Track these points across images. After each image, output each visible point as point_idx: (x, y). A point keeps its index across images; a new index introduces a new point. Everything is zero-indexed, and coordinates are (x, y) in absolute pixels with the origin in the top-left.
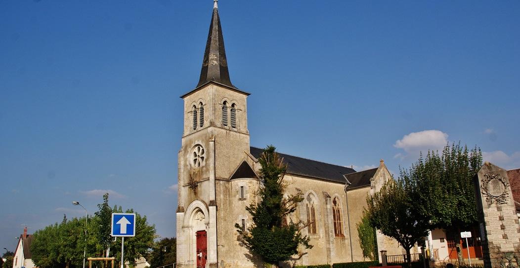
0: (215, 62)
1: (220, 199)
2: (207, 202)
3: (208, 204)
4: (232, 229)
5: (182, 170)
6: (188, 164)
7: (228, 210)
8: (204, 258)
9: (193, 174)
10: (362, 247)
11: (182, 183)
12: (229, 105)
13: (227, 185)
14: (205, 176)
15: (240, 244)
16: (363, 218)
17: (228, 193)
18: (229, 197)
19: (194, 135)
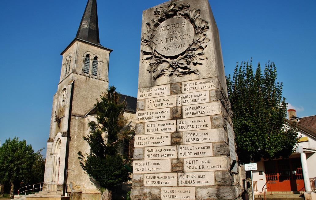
0: (86, 26)
12: (92, 57)
13: (82, 120)
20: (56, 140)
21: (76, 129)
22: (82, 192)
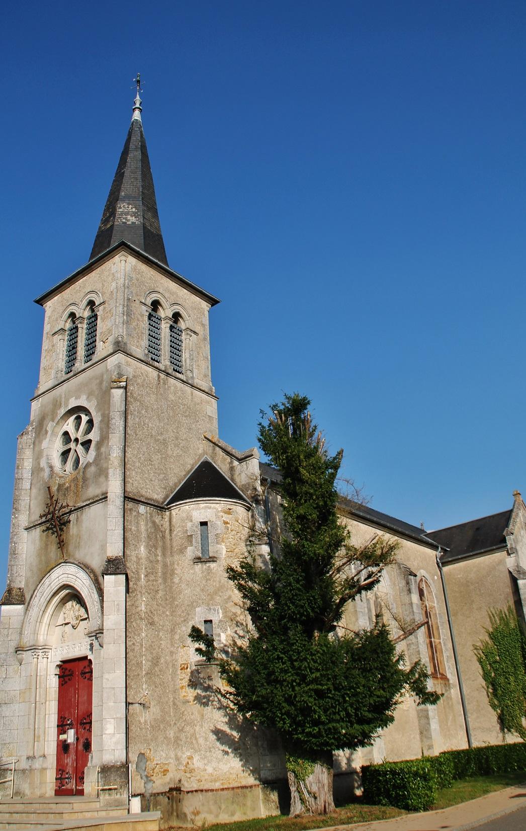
1: (139, 559)
2: (97, 564)
3: (99, 571)
4: (172, 653)
5: (26, 485)
6: (43, 463)
7: (161, 593)
8: (81, 747)
9: (58, 490)
10: (494, 707)
11: (23, 519)
12: (165, 312)
13: (157, 519)
14: (93, 491)
15: (197, 698)
16: (491, 630)
17: (160, 543)
18: (164, 554)
19: (65, 386)
20: (44, 600)
21: (142, 548)
22: (178, 789)
